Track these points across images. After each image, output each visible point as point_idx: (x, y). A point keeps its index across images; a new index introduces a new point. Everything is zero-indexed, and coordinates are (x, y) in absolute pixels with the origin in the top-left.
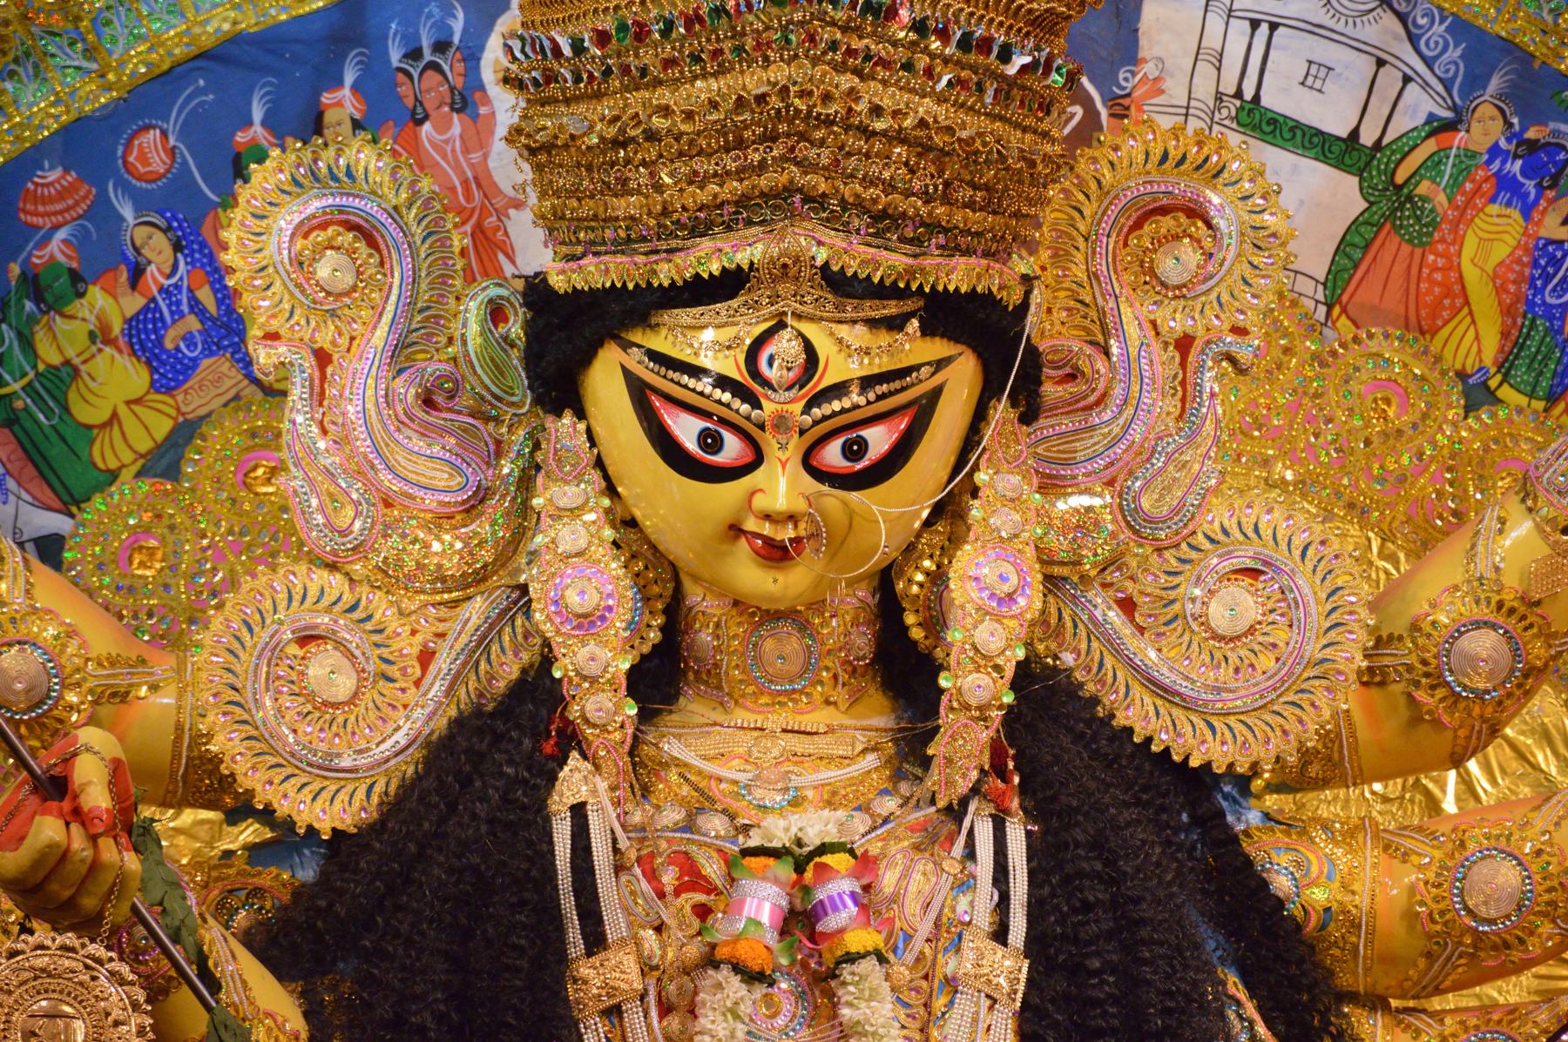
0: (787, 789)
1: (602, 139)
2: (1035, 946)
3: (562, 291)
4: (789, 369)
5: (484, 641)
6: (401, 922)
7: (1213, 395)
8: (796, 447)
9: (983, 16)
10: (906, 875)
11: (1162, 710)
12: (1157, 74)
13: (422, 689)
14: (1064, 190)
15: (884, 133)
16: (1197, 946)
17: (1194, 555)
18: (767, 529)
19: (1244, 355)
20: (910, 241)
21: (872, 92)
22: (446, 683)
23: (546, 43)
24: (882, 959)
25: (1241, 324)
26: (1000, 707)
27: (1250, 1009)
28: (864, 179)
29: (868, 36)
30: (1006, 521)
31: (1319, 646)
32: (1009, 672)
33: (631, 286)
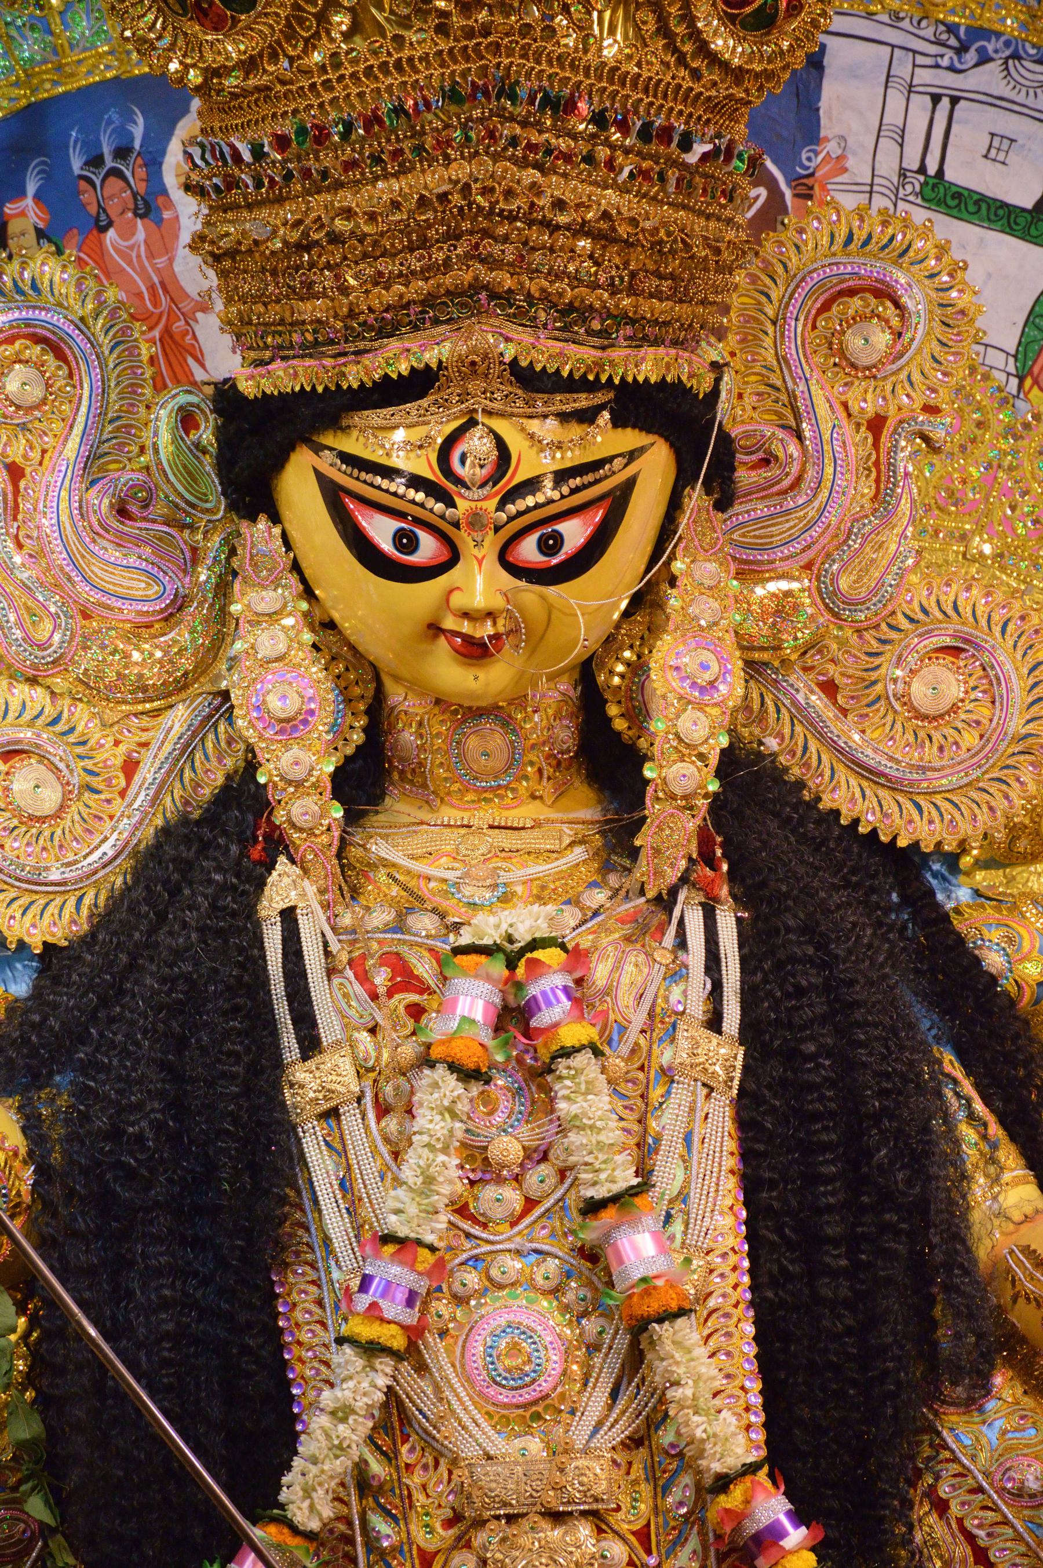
1: (285, 243)
2: (749, 1033)
4: (482, 466)
5: (187, 749)
6: (115, 1034)
11: (868, 792)
12: (839, 152)
13: (127, 799)
15: (568, 227)
16: (911, 1026)
18: (466, 627)
20: (598, 334)
21: (555, 187)
22: (151, 792)
23: (226, 150)
24: (597, 1053)
25: (932, 403)
26: (706, 796)
27: (967, 1087)
28: (549, 273)
29: (548, 130)
30: (705, 609)
32: (714, 760)
33: (320, 389)
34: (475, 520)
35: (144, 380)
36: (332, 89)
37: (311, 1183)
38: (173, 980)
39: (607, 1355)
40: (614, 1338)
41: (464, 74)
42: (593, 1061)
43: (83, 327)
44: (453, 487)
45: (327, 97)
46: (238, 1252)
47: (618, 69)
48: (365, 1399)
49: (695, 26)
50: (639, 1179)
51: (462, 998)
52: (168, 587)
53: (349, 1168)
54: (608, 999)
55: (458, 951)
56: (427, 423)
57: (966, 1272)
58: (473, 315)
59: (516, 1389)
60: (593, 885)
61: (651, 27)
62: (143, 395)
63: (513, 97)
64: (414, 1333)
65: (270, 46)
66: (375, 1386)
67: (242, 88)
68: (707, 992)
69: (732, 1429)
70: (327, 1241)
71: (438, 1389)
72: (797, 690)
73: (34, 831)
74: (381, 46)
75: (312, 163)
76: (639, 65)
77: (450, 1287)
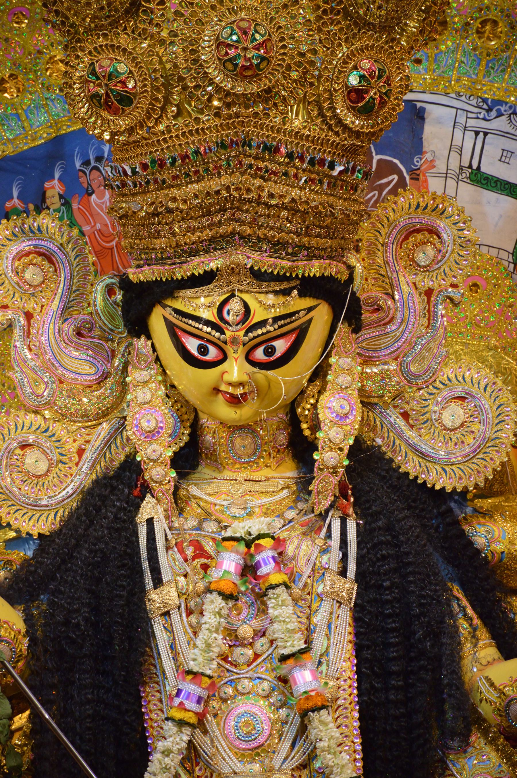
0: (246, 508)
1: (147, 213)
2: (360, 577)
3: (135, 282)
4: (237, 316)
5: (108, 444)
6: (68, 577)
7: (442, 316)
8: (242, 352)
9: (320, 149)
10: (298, 547)
11: (422, 464)
12: (432, 158)
13: (79, 467)
14: (372, 223)
15: (276, 205)
17: (435, 391)
18: (230, 390)
19: (457, 297)
20: (292, 254)
21: (270, 187)
22: (90, 464)
23: (121, 169)
24: (287, 587)
25: (455, 283)
26: (342, 467)
27: (465, 602)
28: (267, 226)
29: (267, 161)
30: (343, 380)
31: (493, 432)
32: (346, 450)
33: (164, 280)
34: (234, 341)
35: (90, 272)
36: (167, 142)
37: (157, 646)
38: (96, 552)
39: (290, 726)
40: (294, 718)
41: (227, 136)
42: (285, 590)
43: (61, 248)
44: (224, 325)
45: (165, 146)
46: (122, 678)
47: (299, 132)
48: (178, 746)
49: (336, 112)
50: (306, 645)
51: (225, 562)
52: (100, 369)
53: (174, 639)
54: (294, 562)
55: (225, 539)
56: (212, 296)
57: (458, 688)
58: (232, 246)
59: (248, 741)
60: (291, 508)
61: (316, 112)
62: (89, 279)
63: (250, 146)
64: (201, 717)
65: (140, 121)
66: (182, 740)
67: (127, 141)
68: (340, 558)
69: (346, 761)
70: (164, 671)
71: (212, 742)
72: (390, 416)
73: (35, 482)
74: (189, 123)
75: (159, 178)
76: (309, 130)
77: (219, 694)
